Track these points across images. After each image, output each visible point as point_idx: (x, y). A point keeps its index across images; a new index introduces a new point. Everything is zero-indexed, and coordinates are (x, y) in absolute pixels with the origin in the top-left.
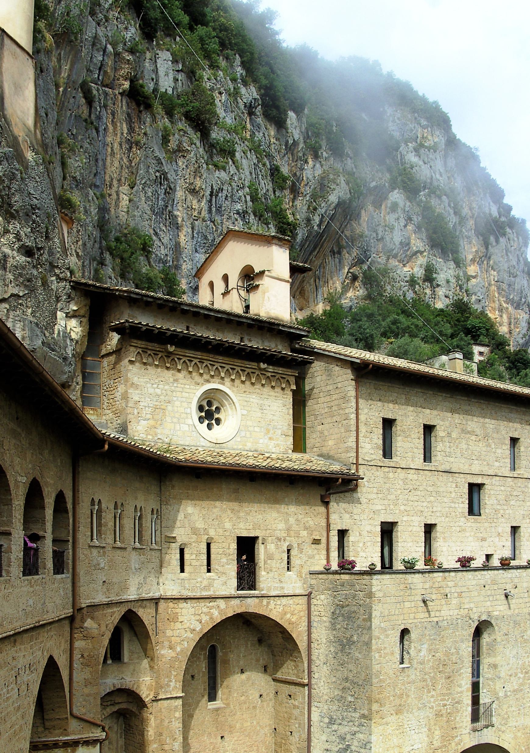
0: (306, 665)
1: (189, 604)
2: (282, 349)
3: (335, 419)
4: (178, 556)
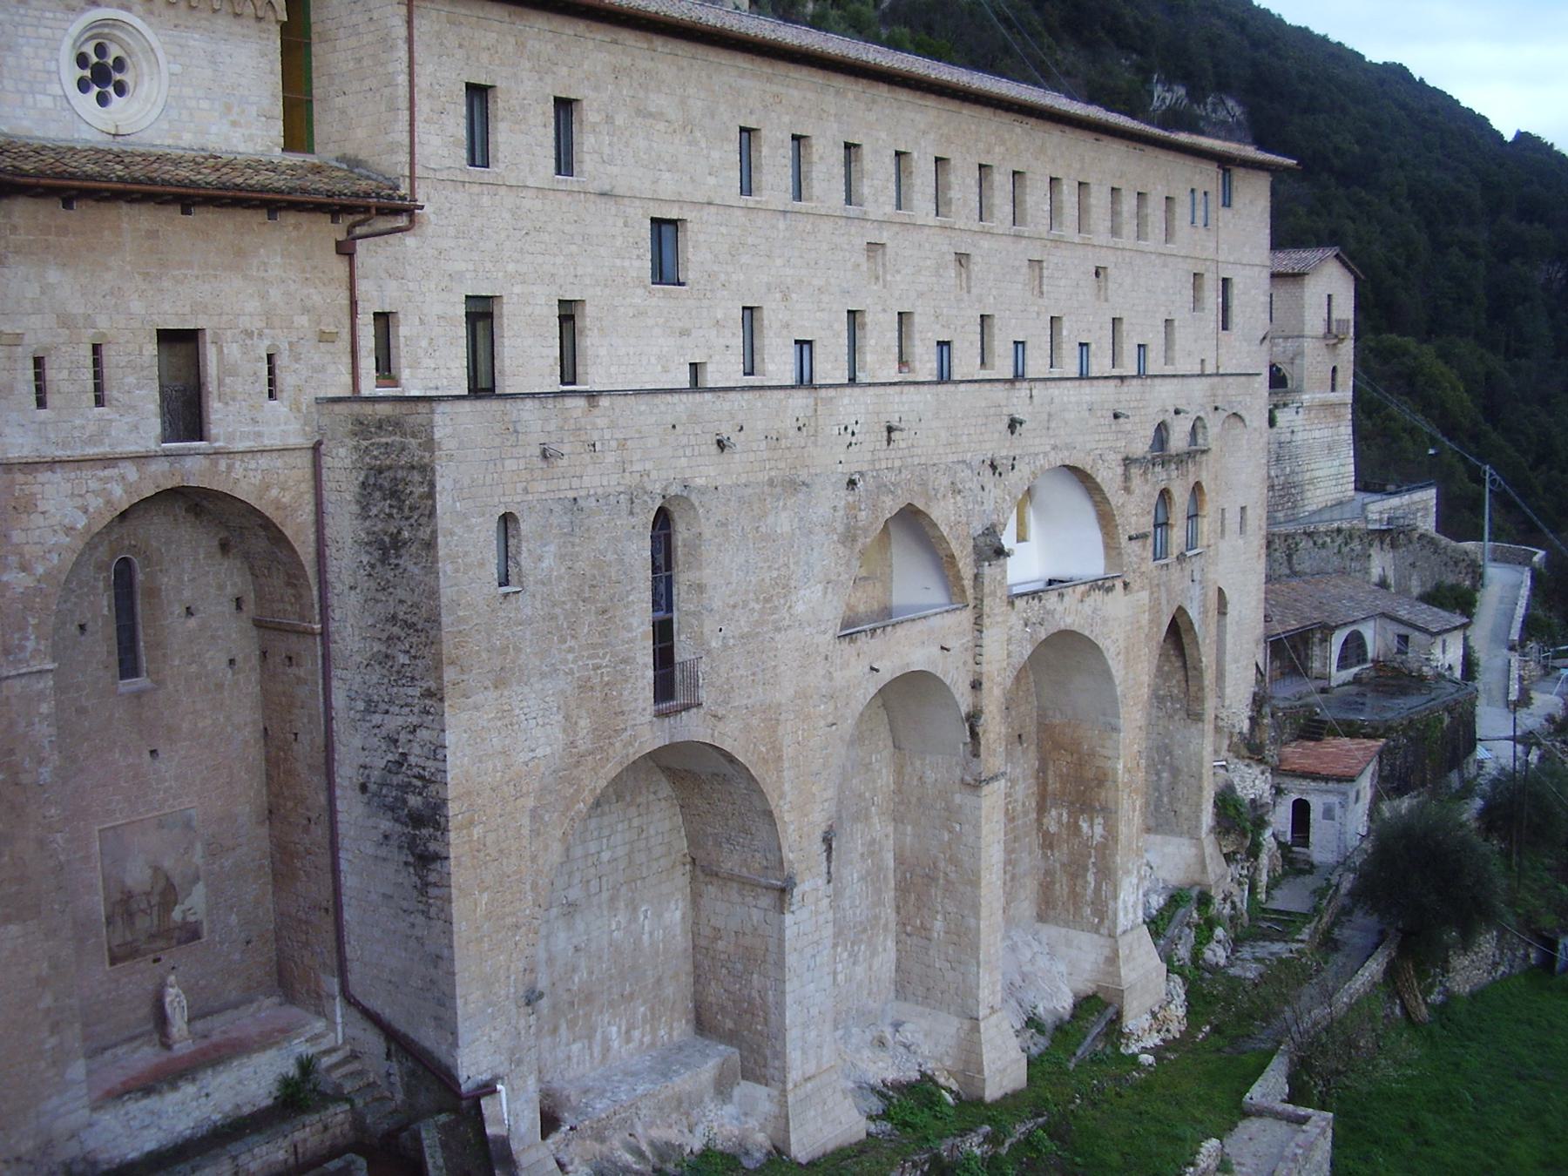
0: (315, 593)
1: (58, 476)
3: (367, 84)
4: (31, 374)
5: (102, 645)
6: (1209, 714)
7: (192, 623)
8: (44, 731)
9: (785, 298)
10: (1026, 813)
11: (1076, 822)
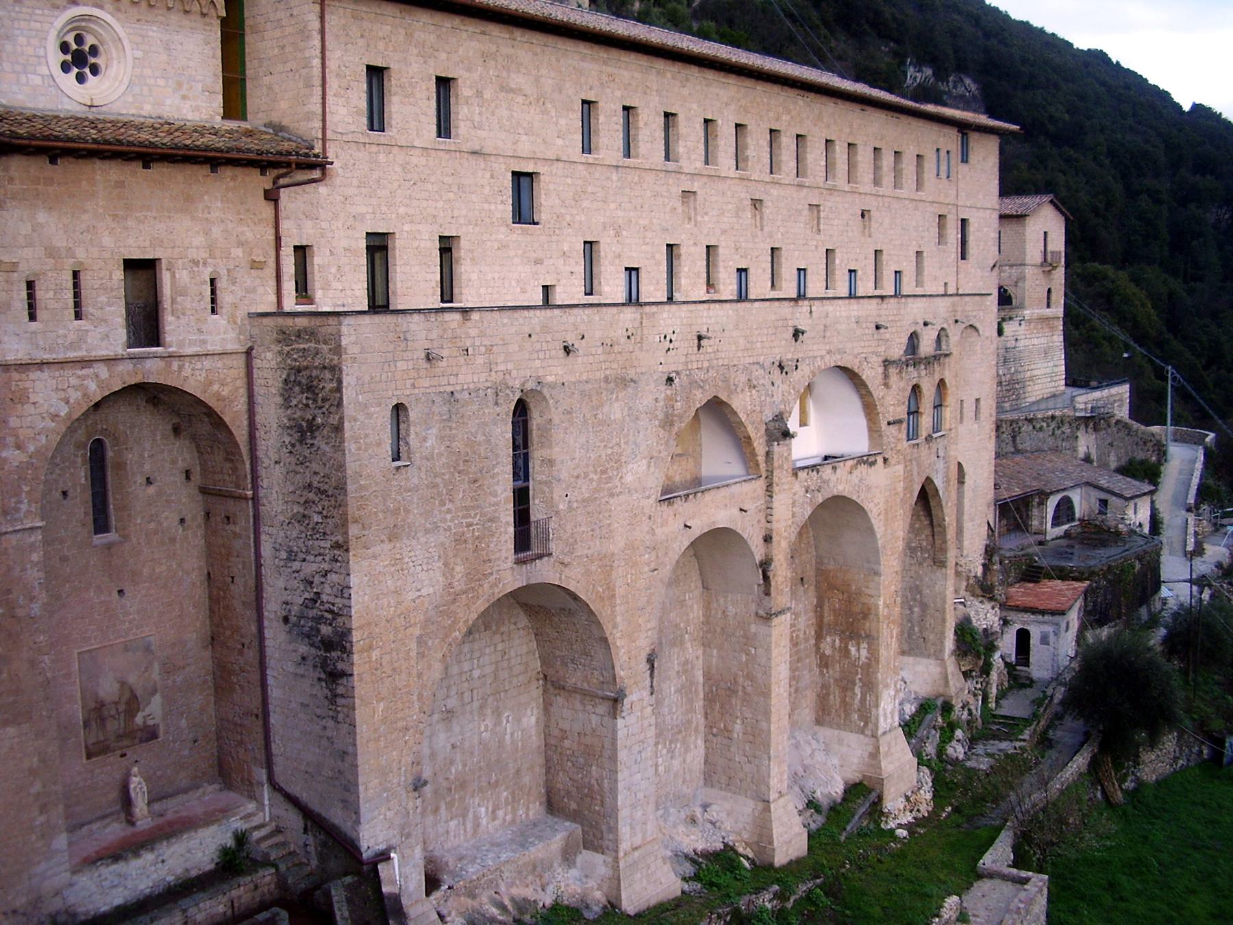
0: (248, 466)
1: (45, 375)
3: (288, 66)
4: (24, 294)
5: (80, 507)
6: (951, 562)
7: (151, 490)
8: (34, 575)
9: (618, 234)
10: (806, 640)
11: (846, 647)
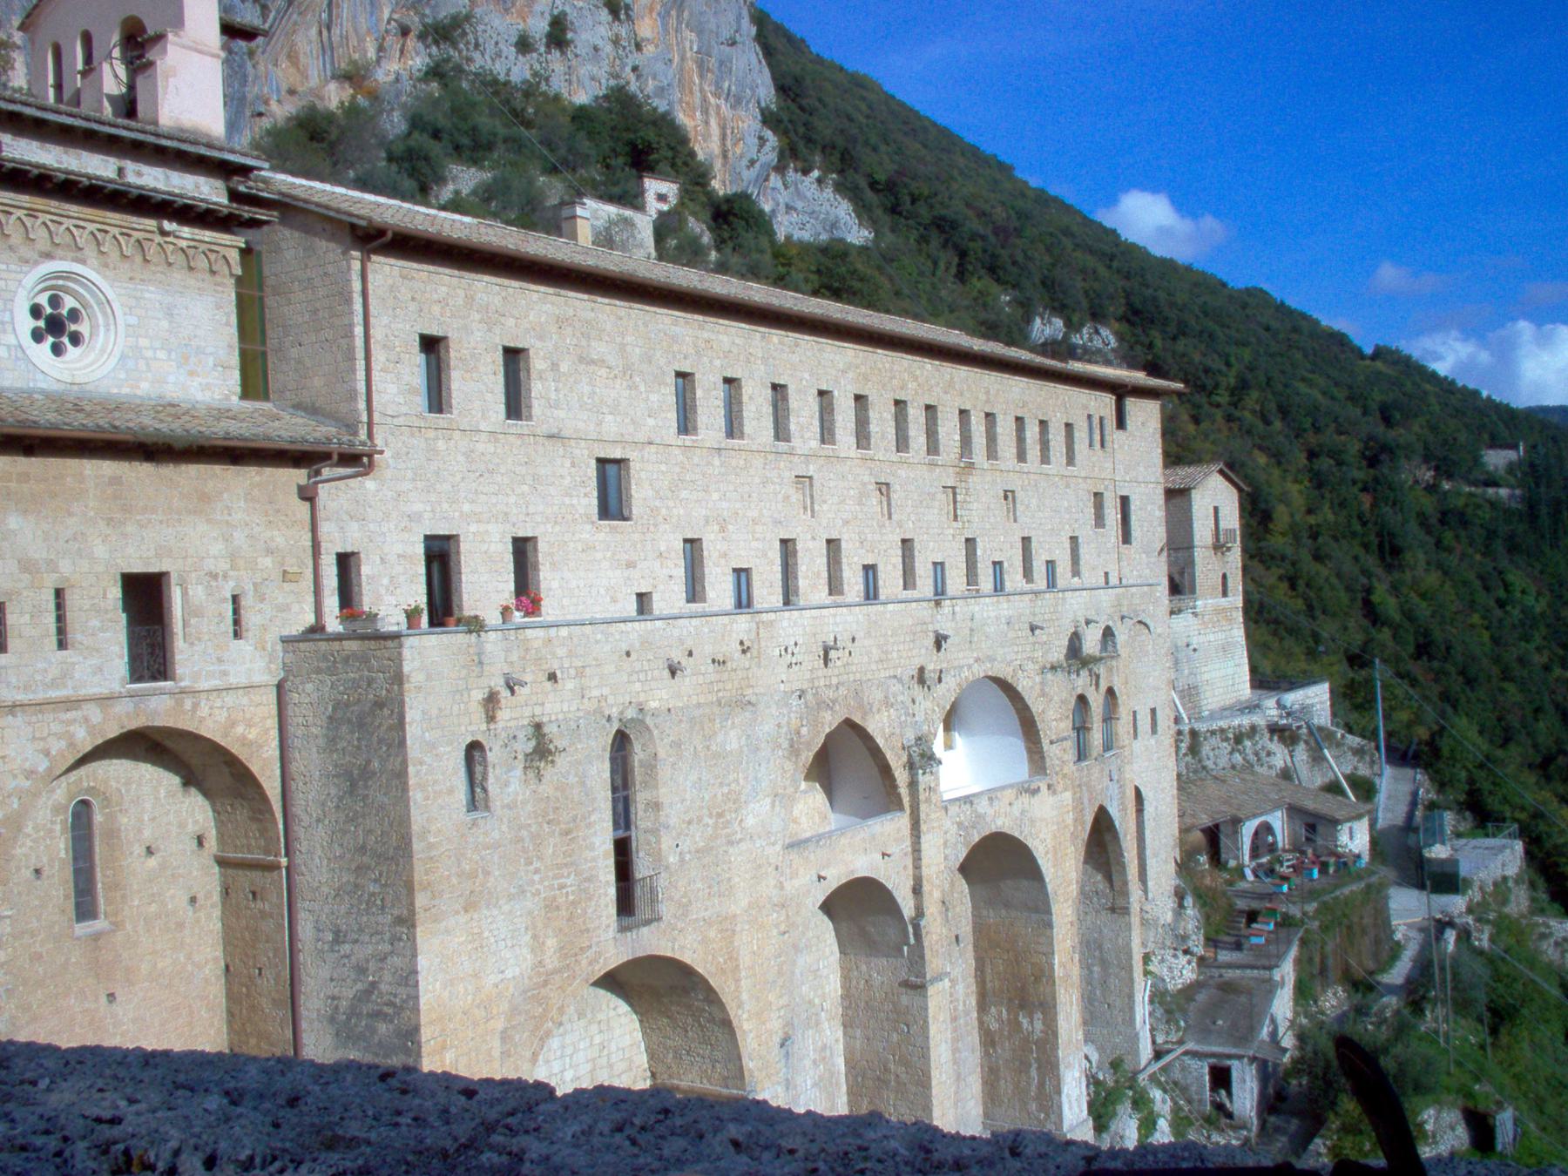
0: (281, 826)
2: (207, 190)
6: (1135, 907)
7: (152, 862)
10: (967, 1013)
11: (1016, 1018)
